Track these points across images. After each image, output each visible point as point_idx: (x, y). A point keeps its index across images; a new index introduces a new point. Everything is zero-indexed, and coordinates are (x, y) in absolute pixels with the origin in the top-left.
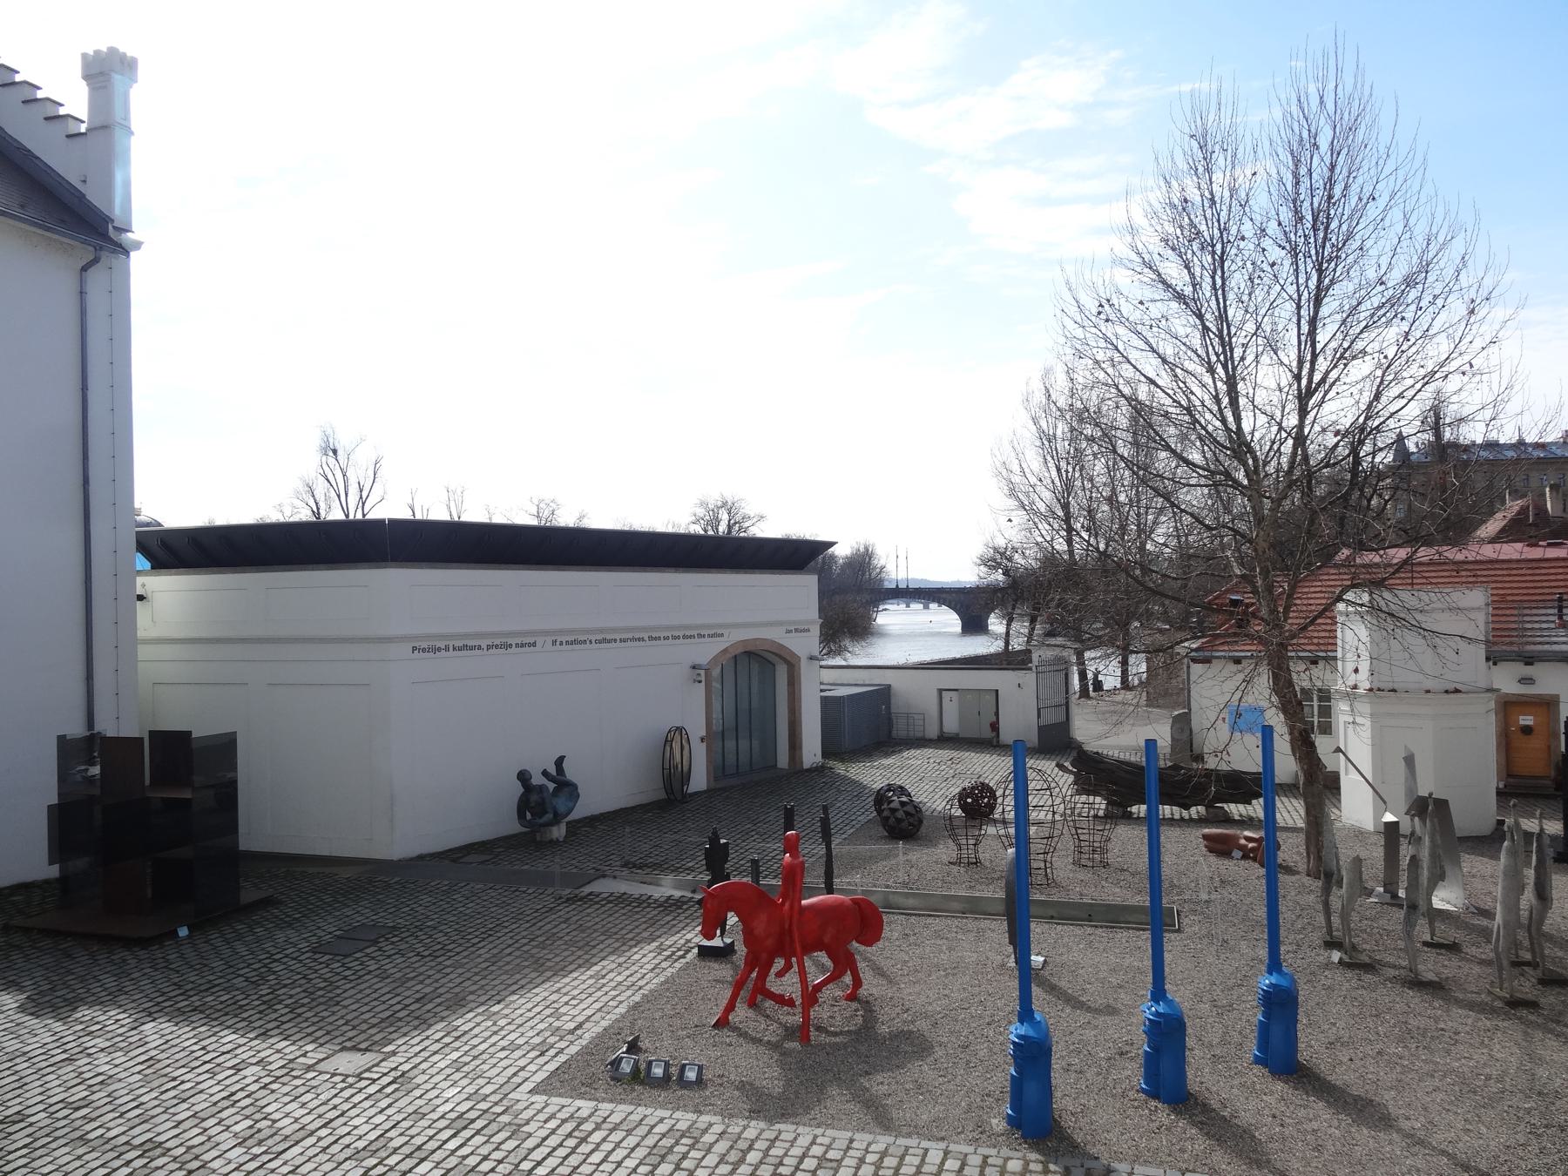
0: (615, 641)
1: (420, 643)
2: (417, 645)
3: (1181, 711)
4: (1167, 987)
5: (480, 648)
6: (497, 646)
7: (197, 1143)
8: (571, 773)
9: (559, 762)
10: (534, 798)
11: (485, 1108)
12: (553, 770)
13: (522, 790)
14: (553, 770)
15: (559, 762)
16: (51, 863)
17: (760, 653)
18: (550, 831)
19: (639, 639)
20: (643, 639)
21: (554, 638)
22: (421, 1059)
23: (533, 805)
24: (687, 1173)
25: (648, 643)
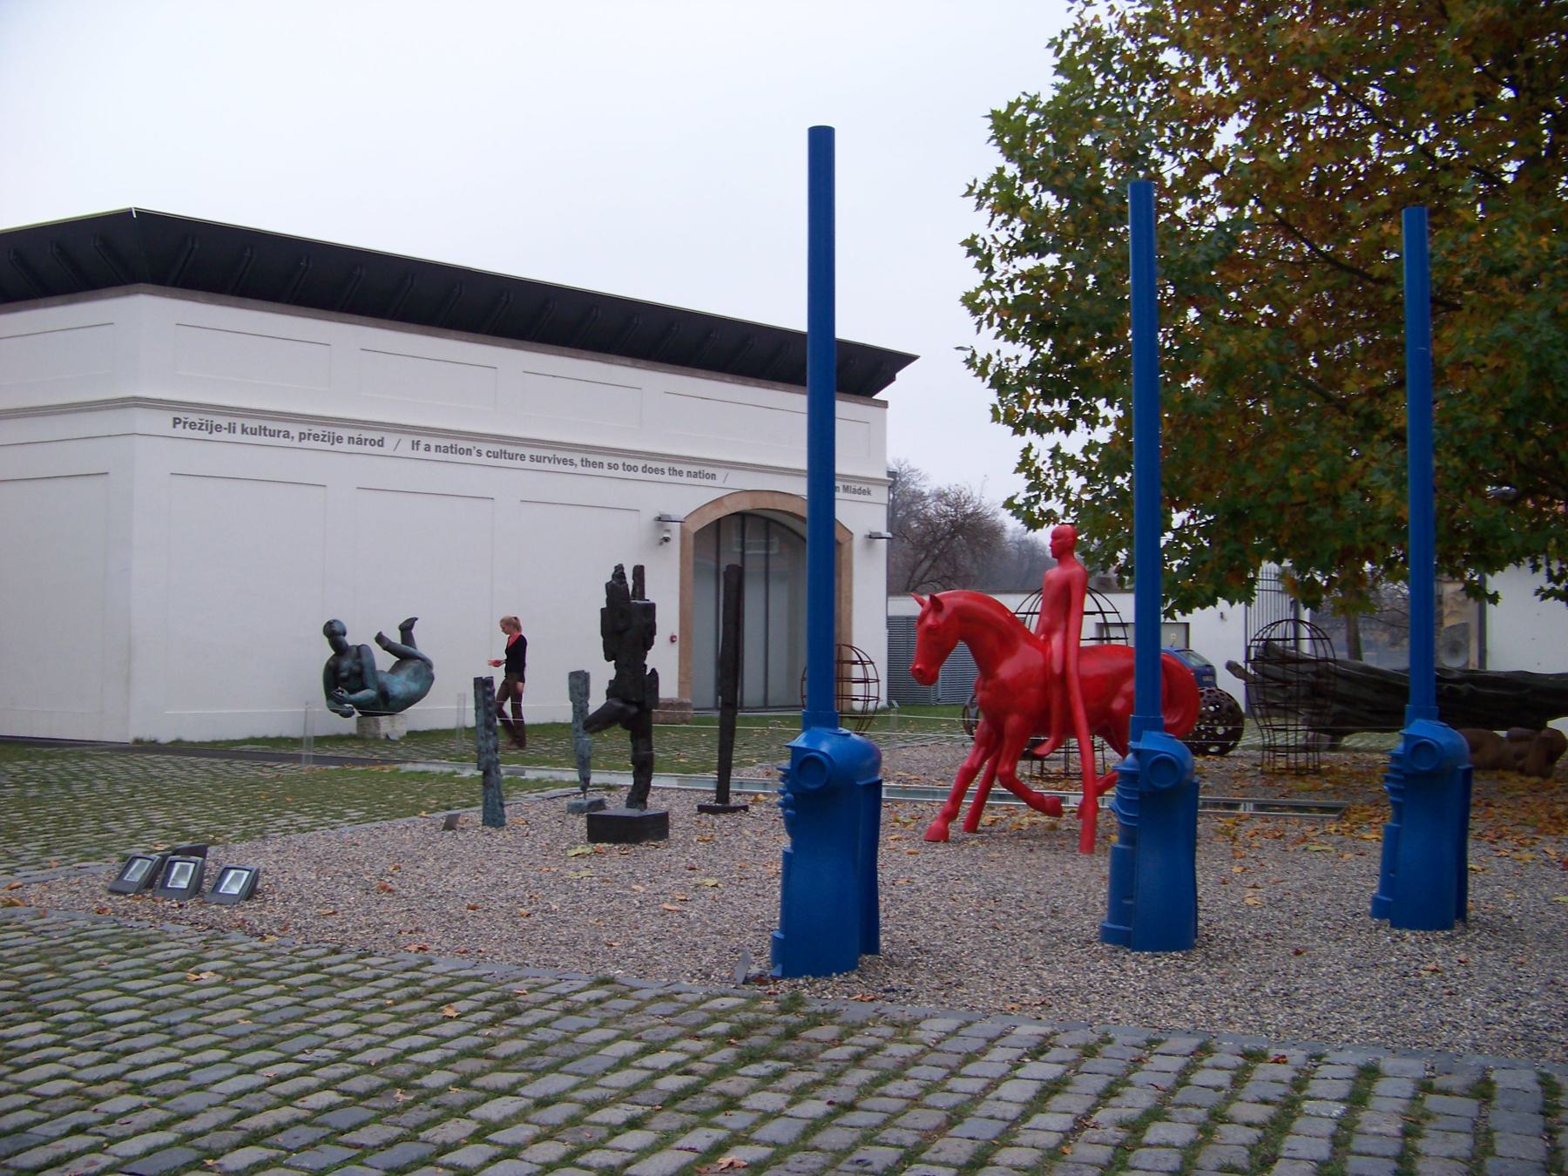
0: (522, 457)
1: (186, 415)
2: (181, 415)
3: (1481, 690)
4: (571, 704)
5: (287, 435)
6: (316, 437)
7: (149, 1061)
8: (423, 643)
9: (406, 628)
10: (346, 663)
11: (915, 1112)
12: (395, 637)
13: (330, 652)
14: (395, 637)
15: (406, 628)
16: (774, 965)
17: (759, 512)
18: (377, 724)
19: (565, 461)
20: (572, 463)
21: (416, 438)
22: (327, 1014)
23: (345, 674)
24: (954, 1171)
25: (580, 469)
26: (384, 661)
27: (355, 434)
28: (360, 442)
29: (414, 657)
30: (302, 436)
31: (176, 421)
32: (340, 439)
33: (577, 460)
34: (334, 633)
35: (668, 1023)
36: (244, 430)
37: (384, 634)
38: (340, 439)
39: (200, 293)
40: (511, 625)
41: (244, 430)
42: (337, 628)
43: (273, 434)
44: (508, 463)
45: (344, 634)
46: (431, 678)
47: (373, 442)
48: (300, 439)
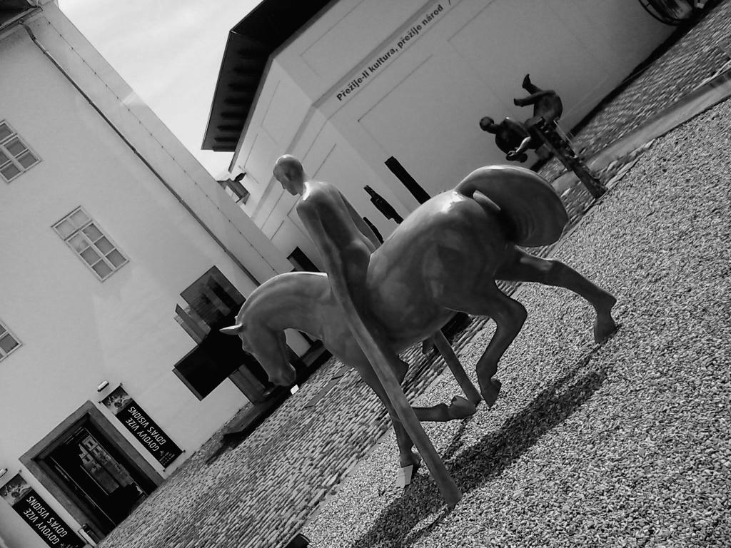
2: (339, 92)
5: (393, 51)
6: (407, 38)
9: (527, 84)
12: (525, 94)
14: (525, 94)
15: (527, 84)
26: (527, 113)
27: (424, 17)
28: (429, 19)
29: (540, 97)
30: (400, 45)
31: (339, 97)
32: (419, 27)
33: (395, 47)
34: (487, 126)
35: (466, 343)
36: (372, 70)
37: (517, 98)
38: (419, 27)
39: (312, 19)
40: (368, 189)
41: (372, 70)
42: (485, 123)
43: (386, 58)
44: (387, 62)
45: (492, 121)
46: (558, 99)
47: (436, 12)
48: (401, 47)
